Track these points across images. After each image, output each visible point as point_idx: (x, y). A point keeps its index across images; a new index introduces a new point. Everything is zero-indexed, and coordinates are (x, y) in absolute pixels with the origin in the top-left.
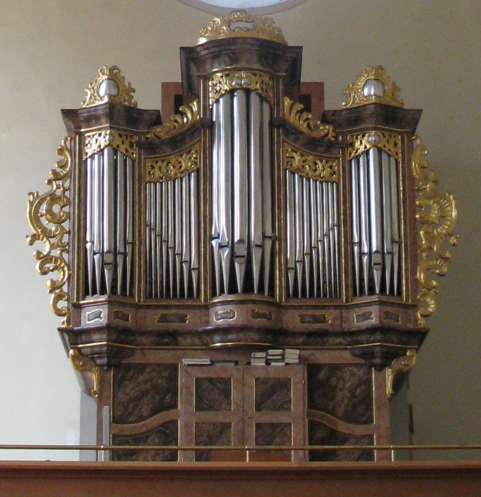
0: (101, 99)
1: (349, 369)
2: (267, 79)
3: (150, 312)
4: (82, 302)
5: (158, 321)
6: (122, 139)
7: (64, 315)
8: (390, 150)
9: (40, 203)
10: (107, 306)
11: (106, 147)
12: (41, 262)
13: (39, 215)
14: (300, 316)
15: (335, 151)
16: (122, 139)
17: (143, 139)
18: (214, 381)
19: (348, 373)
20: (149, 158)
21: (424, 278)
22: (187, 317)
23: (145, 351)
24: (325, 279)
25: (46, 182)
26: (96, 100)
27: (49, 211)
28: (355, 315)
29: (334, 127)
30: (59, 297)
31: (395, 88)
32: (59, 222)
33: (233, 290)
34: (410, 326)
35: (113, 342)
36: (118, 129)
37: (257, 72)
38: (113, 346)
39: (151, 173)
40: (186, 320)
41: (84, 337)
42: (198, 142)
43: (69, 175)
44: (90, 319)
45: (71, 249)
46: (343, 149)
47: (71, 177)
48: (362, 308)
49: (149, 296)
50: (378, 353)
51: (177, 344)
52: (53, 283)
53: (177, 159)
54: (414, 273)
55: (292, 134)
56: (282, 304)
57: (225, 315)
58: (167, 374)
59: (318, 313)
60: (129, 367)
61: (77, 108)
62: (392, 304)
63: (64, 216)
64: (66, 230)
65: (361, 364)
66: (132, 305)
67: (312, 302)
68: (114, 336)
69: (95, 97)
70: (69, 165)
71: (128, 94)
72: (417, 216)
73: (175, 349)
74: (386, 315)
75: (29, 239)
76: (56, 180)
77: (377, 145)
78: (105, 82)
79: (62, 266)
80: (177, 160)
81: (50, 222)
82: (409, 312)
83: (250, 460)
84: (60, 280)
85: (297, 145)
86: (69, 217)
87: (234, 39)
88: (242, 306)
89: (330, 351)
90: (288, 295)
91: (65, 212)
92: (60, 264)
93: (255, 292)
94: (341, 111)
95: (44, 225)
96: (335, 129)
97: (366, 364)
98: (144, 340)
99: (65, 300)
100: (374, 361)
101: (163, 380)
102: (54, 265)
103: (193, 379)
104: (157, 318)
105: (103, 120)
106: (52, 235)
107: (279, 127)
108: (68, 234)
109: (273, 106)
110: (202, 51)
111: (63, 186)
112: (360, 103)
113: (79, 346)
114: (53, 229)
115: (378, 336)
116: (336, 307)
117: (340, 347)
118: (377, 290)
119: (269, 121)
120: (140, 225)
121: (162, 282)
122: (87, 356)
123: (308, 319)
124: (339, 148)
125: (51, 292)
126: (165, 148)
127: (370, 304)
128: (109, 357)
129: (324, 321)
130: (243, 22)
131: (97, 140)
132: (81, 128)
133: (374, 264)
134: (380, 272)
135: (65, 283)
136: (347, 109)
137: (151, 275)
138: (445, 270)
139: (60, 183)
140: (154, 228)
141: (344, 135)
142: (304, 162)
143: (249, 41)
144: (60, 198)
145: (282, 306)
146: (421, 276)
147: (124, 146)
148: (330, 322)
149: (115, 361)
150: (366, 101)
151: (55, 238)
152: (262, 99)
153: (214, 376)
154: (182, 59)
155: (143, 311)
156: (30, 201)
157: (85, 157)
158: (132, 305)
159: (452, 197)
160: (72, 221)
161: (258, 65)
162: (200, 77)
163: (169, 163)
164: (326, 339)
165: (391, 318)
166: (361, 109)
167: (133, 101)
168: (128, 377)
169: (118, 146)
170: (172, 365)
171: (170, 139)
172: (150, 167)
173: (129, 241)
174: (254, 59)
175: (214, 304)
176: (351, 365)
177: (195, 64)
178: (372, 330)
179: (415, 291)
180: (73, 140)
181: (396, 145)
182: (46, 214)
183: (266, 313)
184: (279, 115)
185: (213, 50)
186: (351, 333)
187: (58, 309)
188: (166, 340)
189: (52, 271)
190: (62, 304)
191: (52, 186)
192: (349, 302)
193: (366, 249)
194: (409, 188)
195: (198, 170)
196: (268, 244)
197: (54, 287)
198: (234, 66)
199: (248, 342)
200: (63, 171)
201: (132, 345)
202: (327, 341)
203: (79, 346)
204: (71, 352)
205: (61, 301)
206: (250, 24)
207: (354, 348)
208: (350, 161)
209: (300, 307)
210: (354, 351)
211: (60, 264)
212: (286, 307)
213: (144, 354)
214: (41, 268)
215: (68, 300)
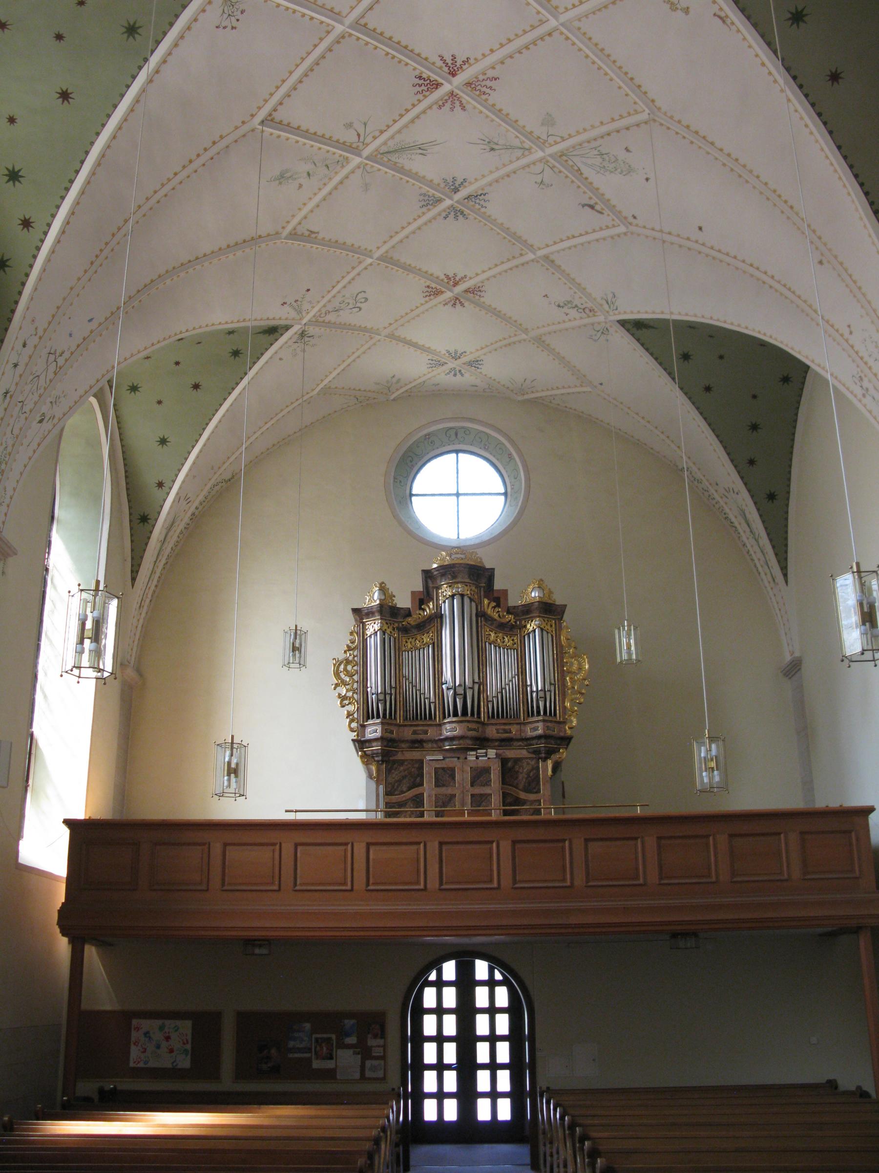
2: (473, 588)
3: (406, 729)
4: (365, 723)
7: (355, 731)
9: (340, 665)
11: (378, 630)
15: (515, 631)
17: (400, 625)
27: (345, 669)
30: (352, 721)
31: (551, 592)
32: (351, 676)
33: (455, 714)
34: (562, 734)
36: (386, 620)
41: (367, 744)
45: (359, 692)
46: (520, 629)
49: (405, 719)
52: (348, 712)
54: (564, 702)
58: (417, 766)
59: (507, 727)
60: (394, 762)
62: (551, 721)
67: (503, 721)
68: (385, 744)
71: (391, 598)
72: (565, 669)
76: (349, 650)
82: (562, 726)
87: (454, 564)
88: (461, 724)
90: (489, 717)
98: (403, 745)
100: (540, 756)
105: (376, 614)
107: (481, 617)
114: (348, 680)
116: (517, 724)
118: (542, 713)
121: (413, 711)
123: (501, 731)
125: (347, 717)
126: (413, 630)
127: (538, 721)
128: (383, 756)
129: (510, 732)
134: (543, 702)
136: (522, 605)
138: (582, 700)
139: (351, 652)
141: (520, 621)
144: (351, 661)
146: (568, 704)
149: (385, 759)
152: (471, 600)
153: (446, 766)
155: (402, 728)
162: (434, 588)
165: (550, 730)
167: (394, 603)
169: (386, 630)
171: (417, 625)
175: (445, 723)
176: (527, 758)
178: (539, 737)
179: (565, 714)
181: (551, 626)
185: (441, 571)
186: (527, 739)
188: (416, 745)
189: (348, 705)
190: (354, 725)
193: (535, 689)
197: (349, 714)
209: (496, 724)
212: (488, 725)
214: (341, 704)
215: (357, 722)
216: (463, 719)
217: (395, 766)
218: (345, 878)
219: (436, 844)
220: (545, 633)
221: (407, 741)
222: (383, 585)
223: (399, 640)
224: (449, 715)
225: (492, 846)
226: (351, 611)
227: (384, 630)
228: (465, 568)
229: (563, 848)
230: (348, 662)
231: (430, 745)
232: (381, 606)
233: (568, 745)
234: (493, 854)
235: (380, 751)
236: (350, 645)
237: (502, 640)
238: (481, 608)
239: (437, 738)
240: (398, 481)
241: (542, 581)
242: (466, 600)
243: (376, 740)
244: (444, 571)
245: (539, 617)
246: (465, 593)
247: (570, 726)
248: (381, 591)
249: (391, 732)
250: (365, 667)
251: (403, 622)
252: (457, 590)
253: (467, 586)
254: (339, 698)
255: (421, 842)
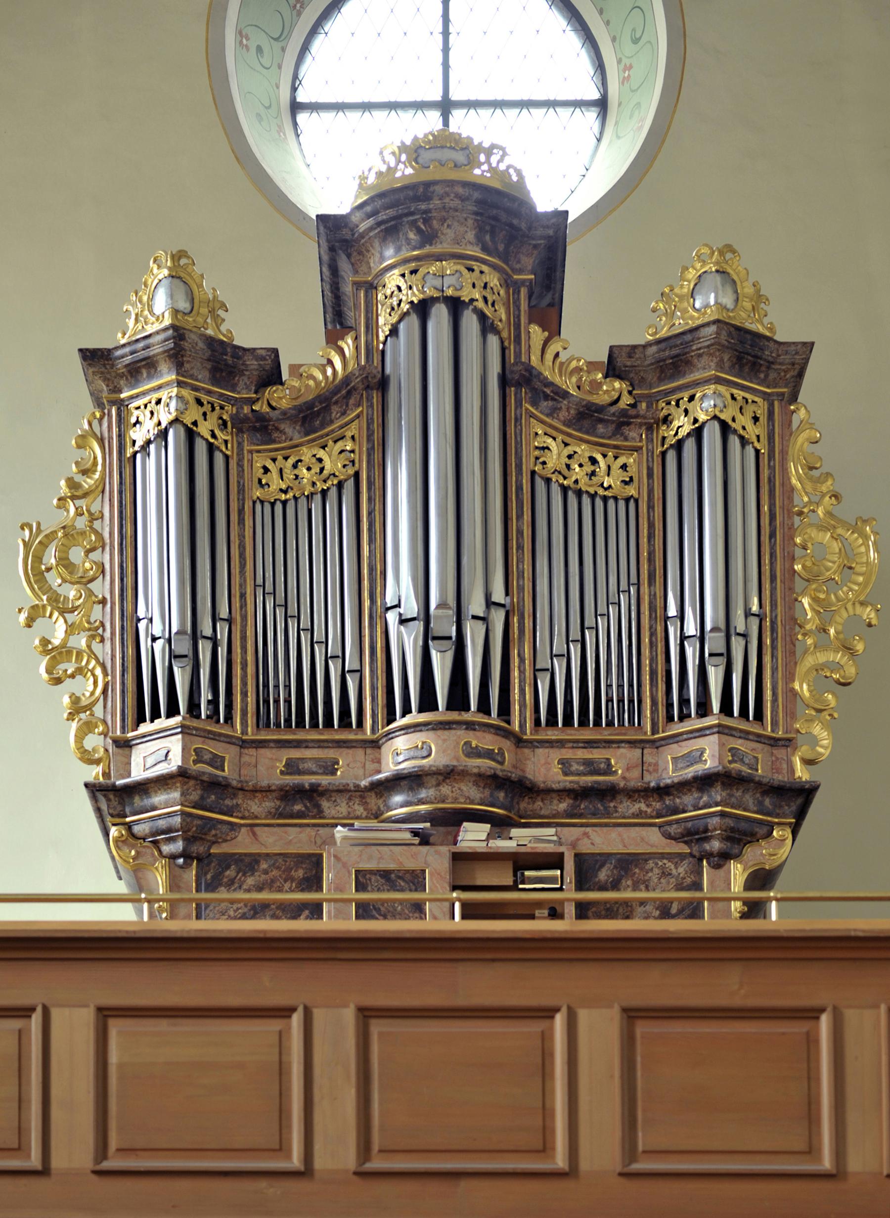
0: (157, 319)
1: (657, 864)
2: (494, 280)
3: (266, 754)
4: (131, 735)
5: (282, 773)
6: (202, 410)
7: (97, 762)
8: (744, 428)
9: (44, 545)
10: (180, 736)
11: (171, 423)
12: (51, 658)
13: (43, 567)
14: (561, 762)
15: (633, 434)
16: (202, 410)
17: (246, 410)
18: (393, 876)
19: (656, 871)
20: (258, 451)
21: (810, 691)
22: (338, 764)
23: (256, 829)
24: (610, 695)
25: (55, 501)
26: (146, 323)
27: (64, 562)
28: (669, 757)
29: (632, 385)
30: (87, 728)
31: (759, 298)
32: (86, 581)
33: (428, 702)
34: (780, 778)
35: (194, 807)
36: (196, 389)
37: (474, 263)
38: (190, 815)
39: (264, 482)
40: (337, 769)
41: (138, 801)
42: (358, 416)
43: (100, 488)
44: (147, 767)
45: (108, 634)
46: (649, 428)
47: (103, 492)
48: (683, 744)
49: (263, 721)
50: (715, 829)
51: (320, 814)
52: (75, 700)
53: (314, 453)
54: (790, 677)
55: (547, 397)
56: (525, 737)
57: (412, 754)
58: (300, 873)
59: (596, 754)
60: (227, 860)
61: (110, 347)
62: (745, 735)
63: (92, 569)
64: (96, 597)
65: (679, 854)
66: (230, 740)
67: (588, 734)
68: (195, 796)
69: (146, 318)
70: (99, 468)
71: (212, 312)
72: (798, 567)
73: (314, 825)
74: (733, 756)
75: (23, 617)
76: (73, 498)
77: (718, 414)
78: (165, 282)
79: (90, 667)
80: (314, 456)
81: (64, 581)
82: (780, 753)
83: (464, 917)
84: (88, 694)
85: (555, 423)
86: (103, 572)
87: (428, 185)
88: (446, 734)
89: (620, 829)
90: (537, 722)
91: (95, 563)
92: (88, 662)
93: (472, 709)
94: (644, 347)
95: (55, 588)
96: (634, 389)
97: (691, 855)
98: (256, 806)
99: (100, 734)
100: (707, 847)
101: (294, 885)
102: (77, 665)
103: (350, 873)
104: (281, 766)
105: (164, 367)
106: (70, 606)
107: (518, 385)
108: (101, 605)
109: (506, 344)
110: (363, 220)
111: (88, 511)
112: (687, 324)
113: (128, 819)
114: (72, 594)
115: (718, 793)
116: (632, 743)
117: (641, 821)
118: (716, 706)
119: (499, 374)
120: (242, 585)
121: (288, 702)
122: (144, 839)
123: (575, 767)
124: (641, 425)
125: (71, 717)
126: (289, 430)
127: (701, 733)
128: (189, 840)
129: (608, 770)
130: (445, 150)
131: (152, 413)
132: (121, 392)
133: (710, 655)
134: (721, 670)
135: (98, 700)
136: (659, 342)
137: (266, 685)
138: (851, 671)
139: (82, 503)
140: (272, 591)
141: (652, 400)
142: (570, 457)
143: (460, 190)
144: (83, 533)
145: (527, 741)
146: (803, 689)
147: (206, 423)
148: (620, 772)
149: (198, 848)
150: (699, 318)
151: (76, 613)
152: (487, 326)
153: (392, 866)
154: (322, 252)
155: (252, 751)
156: (23, 540)
157: (131, 450)
158: (230, 740)
159: (868, 528)
160: (108, 578)
161: (478, 249)
162: (357, 285)
163: (300, 461)
164: (612, 805)
165: (742, 761)
166: (688, 337)
167: (223, 328)
168: (225, 880)
169: (195, 423)
170: (310, 855)
171: (299, 409)
172: (262, 471)
173: (222, 616)
174: (469, 234)
175: (390, 736)
176: (662, 856)
177: (349, 256)
178: (705, 782)
179: (791, 715)
180: (106, 418)
181: (756, 419)
182: (57, 566)
183: (493, 750)
184: (520, 358)
185: (382, 216)
186: (663, 791)
187: (86, 750)
188: (298, 807)
189: (72, 676)
190: (94, 742)
191: (68, 511)
192: (658, 733)
193: (691, 628)
194: (782, 508)
195: (357, 475)
196: (498, 618)
197: (77, 708)
198: (428, 249)
199: (459, 803)
200: (89, 480)
201: (232, 816)
202: (615, 807)
203: (128, 819)
204: (114, 832)
205: (90, 735)
206: (461, 152)
207: (669, 823)
208: (664, 454)
209: (560, 744)
210: (668, 828)
211: (88, 662)
212: (532, 744)
213: (254, 834)
214: (49, 671)
215: (105, 734)
216: (454, 716)
217: (228, 873)
218: (21, 1131)
219: (349, 1015)
220: (734, 442)
221: (267, 791)
222: (183, 261)
223: (240, 465)
224: (406, 711)
225: (552, 1029)
226: (77, 359)
227: (188, 421)
228: (463, 199)
229: (812, 1041)
230: (70, 533)
231: (343, 808)
232: (178, 333)
233: (801, 815)
234: (552, 1055)
235: (178, 819)
236: (79, 478)
237: (589, 468)
238: (518, 355)
239: (364, 783)
240: (253, 50)
241: (734, 252)
242: (470, 323)
243: (163, 782)
244: (391, 212)
245: (718, 381)
246: (465, 295)
247: (809, 756)
248: (176, 281)
249: (217, 762)
250: (129, 551)
251: (254, 401)
252: (438, 283)
253: (470, 269)
254: (46, 652)
255: (293, 1010)
